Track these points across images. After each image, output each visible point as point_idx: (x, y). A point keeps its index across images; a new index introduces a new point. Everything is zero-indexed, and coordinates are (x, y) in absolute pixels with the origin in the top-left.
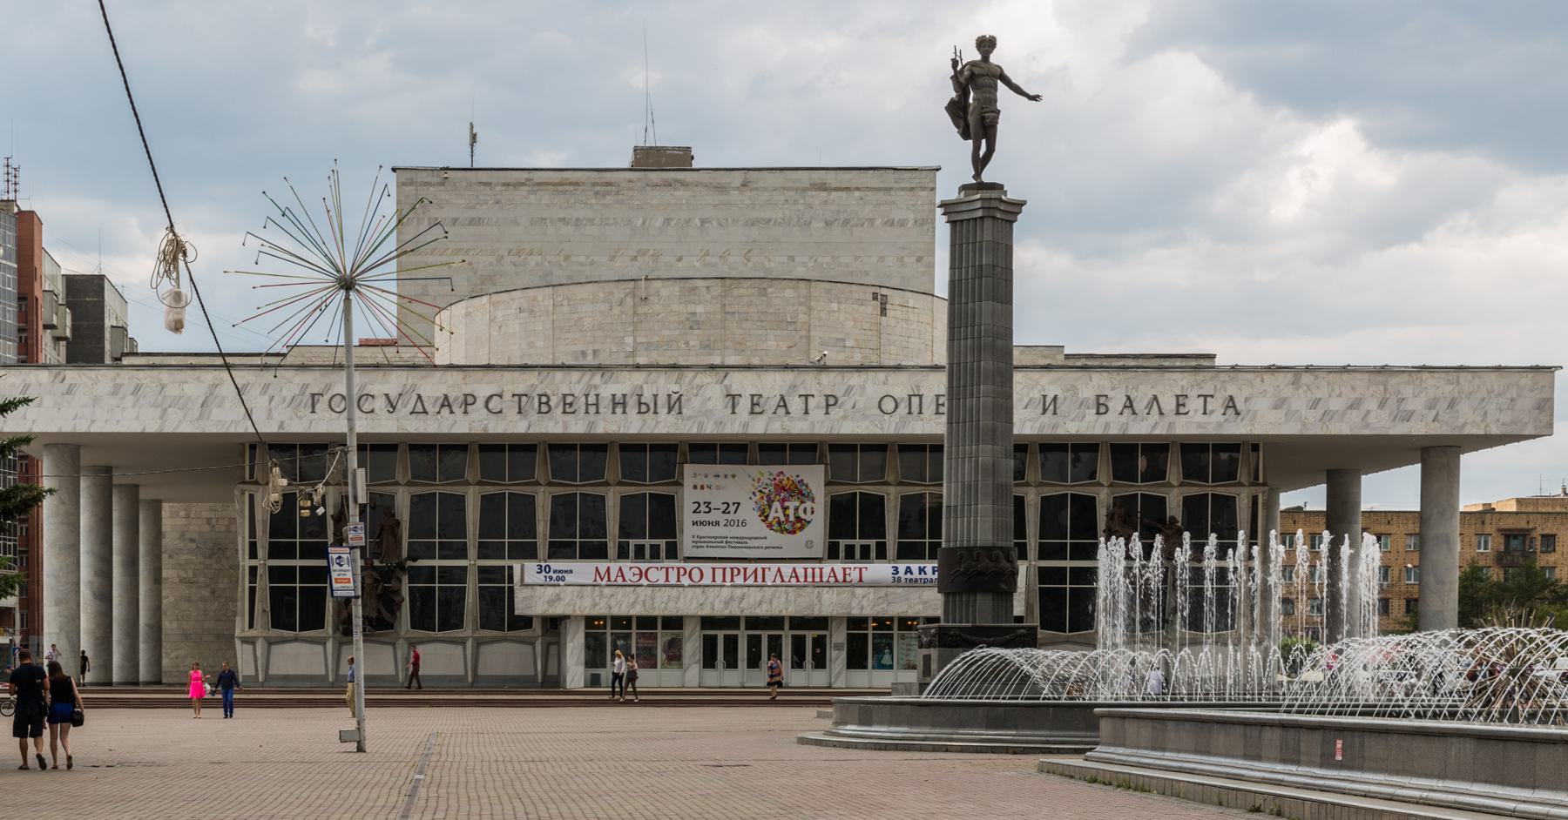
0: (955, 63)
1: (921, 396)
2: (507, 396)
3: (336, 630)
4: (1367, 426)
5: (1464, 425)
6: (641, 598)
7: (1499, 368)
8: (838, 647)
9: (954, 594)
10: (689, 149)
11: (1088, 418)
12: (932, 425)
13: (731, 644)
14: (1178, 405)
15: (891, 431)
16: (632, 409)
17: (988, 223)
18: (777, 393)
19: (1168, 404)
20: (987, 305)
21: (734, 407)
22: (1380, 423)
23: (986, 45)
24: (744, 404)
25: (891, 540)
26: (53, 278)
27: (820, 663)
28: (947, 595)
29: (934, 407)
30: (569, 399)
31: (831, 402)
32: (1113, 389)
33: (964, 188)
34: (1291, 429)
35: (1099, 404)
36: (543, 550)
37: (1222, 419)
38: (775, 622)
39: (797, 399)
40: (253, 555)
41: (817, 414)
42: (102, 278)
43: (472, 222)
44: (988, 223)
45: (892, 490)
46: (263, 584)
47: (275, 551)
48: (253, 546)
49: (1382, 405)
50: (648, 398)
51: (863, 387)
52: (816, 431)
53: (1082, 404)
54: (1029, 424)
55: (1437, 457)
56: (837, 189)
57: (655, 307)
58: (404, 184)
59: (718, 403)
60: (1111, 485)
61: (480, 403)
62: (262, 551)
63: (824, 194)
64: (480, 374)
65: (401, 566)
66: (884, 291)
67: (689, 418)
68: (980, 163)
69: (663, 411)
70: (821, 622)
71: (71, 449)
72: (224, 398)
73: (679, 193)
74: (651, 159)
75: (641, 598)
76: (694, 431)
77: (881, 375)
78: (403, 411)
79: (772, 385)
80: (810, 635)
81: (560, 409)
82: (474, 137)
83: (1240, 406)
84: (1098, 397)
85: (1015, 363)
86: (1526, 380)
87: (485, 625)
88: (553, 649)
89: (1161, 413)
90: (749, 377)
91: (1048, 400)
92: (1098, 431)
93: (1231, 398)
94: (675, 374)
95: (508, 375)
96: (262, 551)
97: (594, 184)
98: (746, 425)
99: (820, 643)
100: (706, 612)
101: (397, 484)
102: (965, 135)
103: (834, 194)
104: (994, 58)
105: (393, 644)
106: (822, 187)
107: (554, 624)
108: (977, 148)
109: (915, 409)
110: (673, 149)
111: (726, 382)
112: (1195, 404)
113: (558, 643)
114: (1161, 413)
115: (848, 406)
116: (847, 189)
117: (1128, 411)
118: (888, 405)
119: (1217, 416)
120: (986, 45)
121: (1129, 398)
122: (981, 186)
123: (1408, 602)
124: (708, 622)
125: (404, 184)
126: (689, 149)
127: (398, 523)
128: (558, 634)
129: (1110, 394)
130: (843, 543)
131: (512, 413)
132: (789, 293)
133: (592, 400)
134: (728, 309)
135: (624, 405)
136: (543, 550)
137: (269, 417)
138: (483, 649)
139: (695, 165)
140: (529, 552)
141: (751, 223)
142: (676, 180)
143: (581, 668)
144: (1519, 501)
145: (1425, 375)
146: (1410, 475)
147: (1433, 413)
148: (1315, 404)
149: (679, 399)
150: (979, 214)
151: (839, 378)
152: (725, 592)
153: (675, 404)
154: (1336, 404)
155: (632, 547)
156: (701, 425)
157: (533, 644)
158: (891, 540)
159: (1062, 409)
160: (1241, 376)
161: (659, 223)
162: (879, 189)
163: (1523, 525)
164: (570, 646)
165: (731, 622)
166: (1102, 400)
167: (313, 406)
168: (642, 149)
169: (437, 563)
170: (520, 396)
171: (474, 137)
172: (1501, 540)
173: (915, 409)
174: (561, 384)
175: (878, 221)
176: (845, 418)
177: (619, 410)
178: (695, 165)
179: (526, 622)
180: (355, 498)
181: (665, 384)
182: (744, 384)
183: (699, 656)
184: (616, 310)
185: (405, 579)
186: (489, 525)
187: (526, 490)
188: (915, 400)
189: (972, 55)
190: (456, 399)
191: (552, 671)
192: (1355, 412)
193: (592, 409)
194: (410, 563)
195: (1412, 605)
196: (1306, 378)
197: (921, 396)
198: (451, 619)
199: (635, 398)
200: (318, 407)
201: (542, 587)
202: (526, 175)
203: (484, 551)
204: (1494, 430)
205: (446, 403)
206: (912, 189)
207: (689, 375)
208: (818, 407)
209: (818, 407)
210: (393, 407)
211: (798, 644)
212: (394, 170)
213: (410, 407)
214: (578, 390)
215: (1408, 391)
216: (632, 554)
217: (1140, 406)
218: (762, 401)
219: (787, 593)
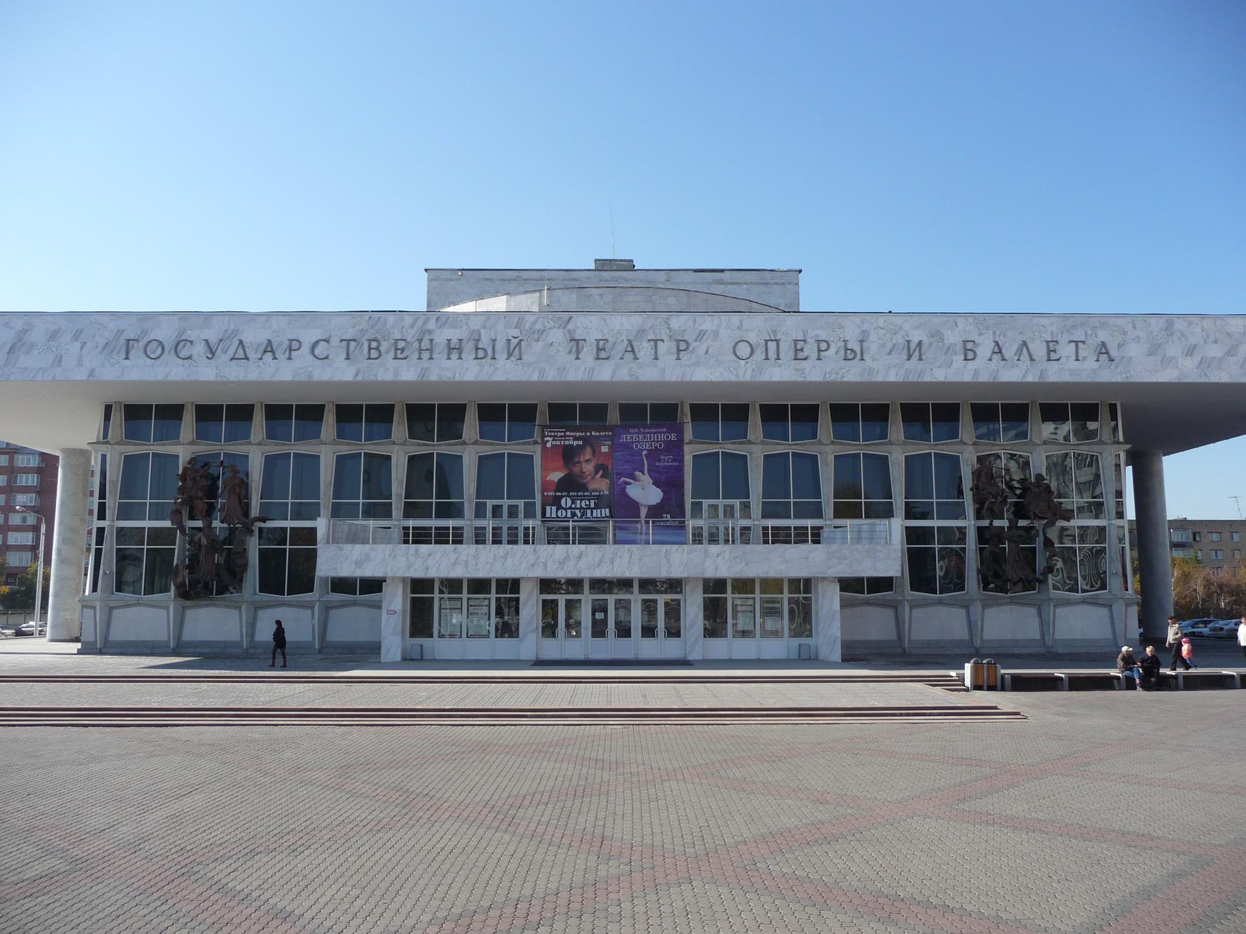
1: (777, 341)
2: (335, 341)
11: (955, 365)
14: (1049, 351)
15: (748, 378)
16: (468, 354)
19: (1039, 350)
21: (578, 352)
27: (674, 632)
29: (792, 353)
30: (401, 344)
31: (682, 347)
32: (980, 334)
35: (966, 350)
37: (1096, 365)
38: (575, 584)
39: (645, 344)
50: (485, 342)
51: (716, 333)
52: (667, 379)
53: (949, 349)
54: (893, 372)
60: (975, 444)
61: (305, 349)
67: (530, 364)
69: (502, 356)
70: (674, 585)
72: (32, 346)
74: (604, 265)
76: (535, 378)
78: (222, 358)
81: (392, 354)
83: (1114, 353)
84: (965, 342)
87: (264, 588)
89: (1032, 359)
91: (913, 346)
92: (967, 378)
93: (1104, 344)
99: (673, 611)
111: (570, 326)
112: (1066, 350)
114: (1032, 359)
115: (701, 351)
117: (996, 357)
118: (744, 350)
119: (1091, 363)
121: (997, 344)
124: (547, 585)
129: (978, 339)
131: (339, 359)
133: (425, 344)
135: (460, 350)
137: (80, 364)
138: (333, 613)
143: (398, 639)
149: (519, 344)
155: (705, 507)
156: (542, 372)
157: (312, 608)
159: (928, 355)
166: (969, 346)
167: (127, 353)
169: (289, 524)
170: (349, 341)
176: (698, 363)
177: (455, 355)
188: (772, 345)
190: (279, 345)
192: (1231, 359)
193: (426, 355)
195: (997, 575)
197: (777, 341)
198: (955, 582)
199: (472, 343)
200: (132, 353)
202: (517, 273)
205: (269, 348)
210: (212, 352)
213: (231, 353)
217: (1009, 352)
218: (608, 346)
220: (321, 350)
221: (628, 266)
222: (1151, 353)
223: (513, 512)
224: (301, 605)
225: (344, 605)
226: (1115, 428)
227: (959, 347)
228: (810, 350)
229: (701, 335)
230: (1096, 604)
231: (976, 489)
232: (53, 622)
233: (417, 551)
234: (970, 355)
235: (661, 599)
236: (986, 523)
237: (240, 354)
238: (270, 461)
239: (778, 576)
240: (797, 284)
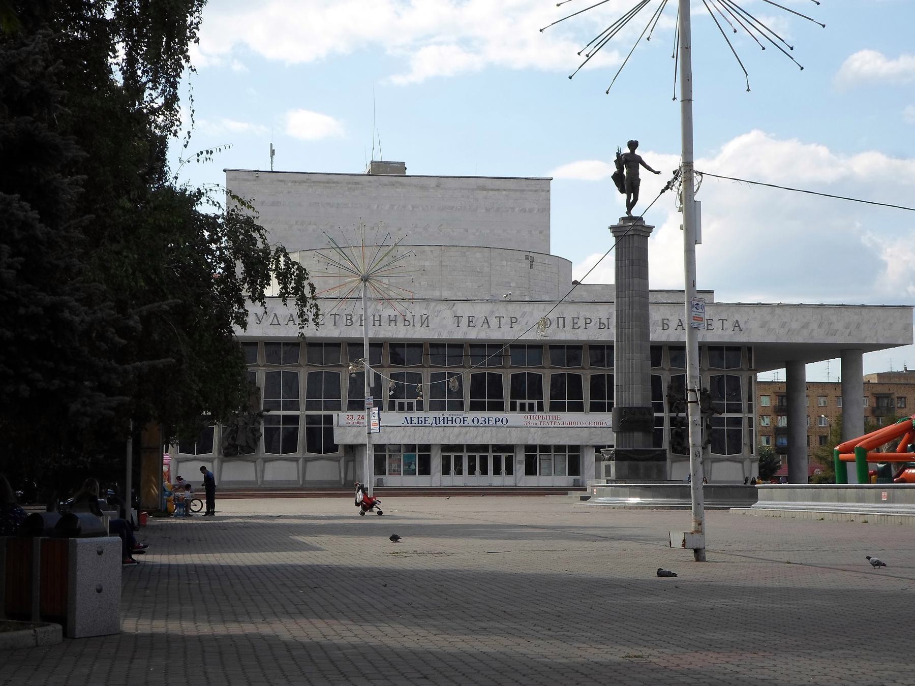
3: (220, 453)
4: (812, 338)
5: (866, 337)
6: (408, 434)
7: (883, 306)
8: (520, 462)
9: (621, 432)
10: (404, 163)
13: (484, 460)
17: (636, 237)
18: (483, 315)
20: (636, 281)
22: (819, 337)
23: (633, 145)
24: (464, 322)
25: (546, 400)
27: (510, 471)
28: (617, 433)
31: (513, 321)
33: (623, 219)
34: (770, 339)
36: (345, 405)
37: (732, 333)
43: (274, 204)
44: (636, 237)
45: (546, 371)
46: (744, 404)
47: (738, 421)
49: (820, 326)
50: (409, 317)
51: (532, 313)
55: (850, 355)
56: (492, 190)
58: (231, 180)
59: (449, 321)
60: (670, 370)
63: (485, 192)
65: (260, 415)
66: (532, 255)
67: (433, 329)
68: (630, 206)
69: (418, 325)
70: (510, 448)
73: (399, 190)
75: (408, 434)
77: (542, 306)
79: (480, 311)
80: (503, 456)
82: (273, 152)
86: (897, 313)
88: (351, 464)
90: (467, 305)
92: (664, 339)
94: (424, 304)
96: (745, 422)
97: (348, 183)
98: (465, 333)
100: (446, 442)
101: (258, 365)
102: (622, 191)
103: (491, 192)
104: (637, 152)
105: (255, 462)
106: (484, 189)
107: (353, 450)
109: (561, 325)
110: (394, 163)
113: (354, 461)
115: (524, 323)
116: (499, 190)
120: (633, 145)
122: (631, 218)
123: (821, 438)
124: (446, 448)
125: (231, 180)
126: (404, 163)
127: (259, 389)
128: (354, 455)
130: (518, 402)
132: (478, 255)
134: (444, 264)
136: (345, 405)
139: (408, 173)
140: (338, 407)
142: (397, 182)
144: (879, 375)
145: (843, 310)
146: (835, 365)
147: (848, 331)
148: (783, 325)
150: (631, 233)
151: (518, 308)
152: (456, 430)
153: (425, 321)
154: (795, 325)
155: (518, 404)
156: (440, 333)
157: (339, 461)
158: (507, 399)
160: (742, 309)
161: (387, 207)
162: (517, 190)
163: (887, 391)
165: (458, 448)
168: (376, 162)
171: (273, 152)
172: (874, 400)
173: (561, 325)
175: (517, 209)
177: (393, 324)
178: (408, 173)
180: (369, 385)
181: (419, 310)
182: (464, 310)
183: (440, 468)
185: (262, 422)
187: (497, 371)
188: (561, 320)
191: (350, 477)
193: (377, 323)
194: (265, 413)
196: (778, 311)
198: (290, 445)
201: (348, 426)
204: (882, 341)
206: (536, 191)
207: (433, 304)
208: (506, 324)
209: (506, 324)
211: (497, 461)
212: (225, 171)
216: (518, 408)
218: (474, 320)
219: (491, 431)
221: (398, 169)
226: (750, 359)
227: (660, 322)
228: (581, 323)
229: (524, 314)
230: (735, 461)
231: (669, 396)
234: (666, 327)
235: (478, 456)
236: (674, 415)
237: (275, 322)
238: (269, 376)
239: (427, 443)
240: (549, 191)
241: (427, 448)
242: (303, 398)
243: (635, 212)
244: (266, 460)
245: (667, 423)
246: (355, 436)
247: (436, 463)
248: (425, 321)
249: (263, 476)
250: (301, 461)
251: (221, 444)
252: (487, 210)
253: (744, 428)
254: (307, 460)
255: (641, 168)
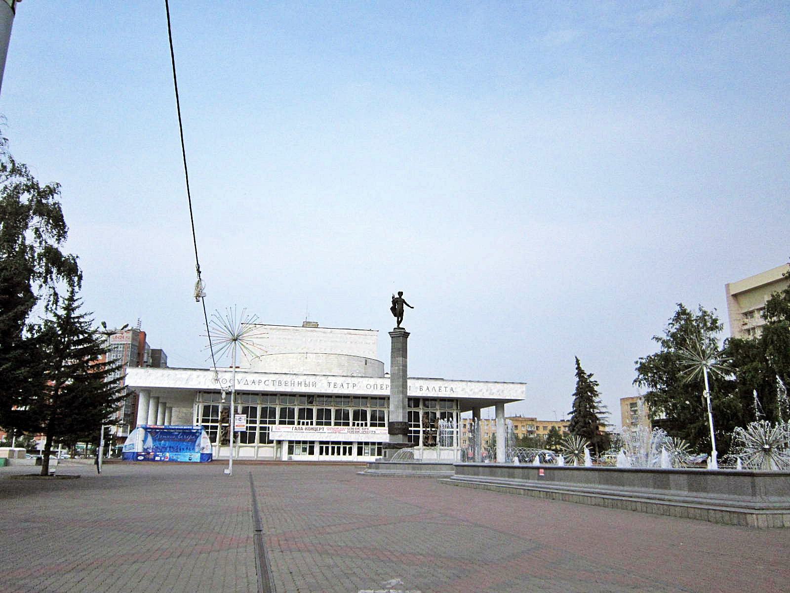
0: (393, 298)
12: (386, 392)
13: (339, 448)
19: (437, 389)
23: (400, 294)
24: (332, 385)
26: (148, 350)
27: (350, 454)
31: (354, 385)
33: (395, 329)
38: (339, 443)
40: (198, 422)
41: (351, 388)
42: (161, 350)
45: (369, 409)
47: (203, 421)
48: (198, 420)
49: (487, 391)
50: (307, 383)
53: (417, 388)
57: (309, 360)
59: (326, 385)
62: (200, 421)
64: (264, 375)
68: (399, 323)
69: (311, 386)
70: (351, 443)
71: (149, 392)
78: (242, 384)
79: (339, 380)
80: (348, 446)
85: (389, 380)
88: (279, 449)
94: (314, 377)
95: (271, 375)
96: (200, 421)
97: (294, 330)
99: (350, 449)
100: (321, 440)
102: (395, 316)
104: (403, 297)
107: (279, 442)
108: (398, 320)
112: (443, 389)
118: (369, 386)
119: (449, 393)
120: (400, 294)
124: (321, 442)
130: (302, 421)
133: (292, 383)
140: (274, 423)
141: (332, 342)
145: (496, 384)
148: (471, 390)
153: (314, 384)
154: (476, 390)
161: (309, 340)
164: (284, 449)
174: (284, 378)
176: (358, 389)
177: (300, 385)
179: (272, 442)
181: (312, 379)
184: (299, 360)
186: (263, 415)
187: (382, 409)
188: (375, 386)
189: (397, 296)
191: (278, 455)
193: (293, 385)
198: (252, 441)
203: (261, 422)
204: (513, 398)
207: (318, 377)
214: (289, 380)
215: (492, 388)
220: (267, 383)
222: (463, 390)
223: (307, 423)
224: (252, 447)
225: (263, 447)
229: (359, 383)
231: (422, 421)
232: (716, 446)
233: (385, 434)
235: (324, 446)
236: (424, 429)
241: (313, 442)
242: (258, 419)
243: (401, 326)
244: (240, 447)
245: (421, 432)
246: (326, 438)
247: (317, 449)
248: (314, 384)
249: (257, 454)
250: (256, 448)
251: (220, 439)
252: (351, 342)
253: (455, 435)
254: (259, 447)
255: (404, 304)
